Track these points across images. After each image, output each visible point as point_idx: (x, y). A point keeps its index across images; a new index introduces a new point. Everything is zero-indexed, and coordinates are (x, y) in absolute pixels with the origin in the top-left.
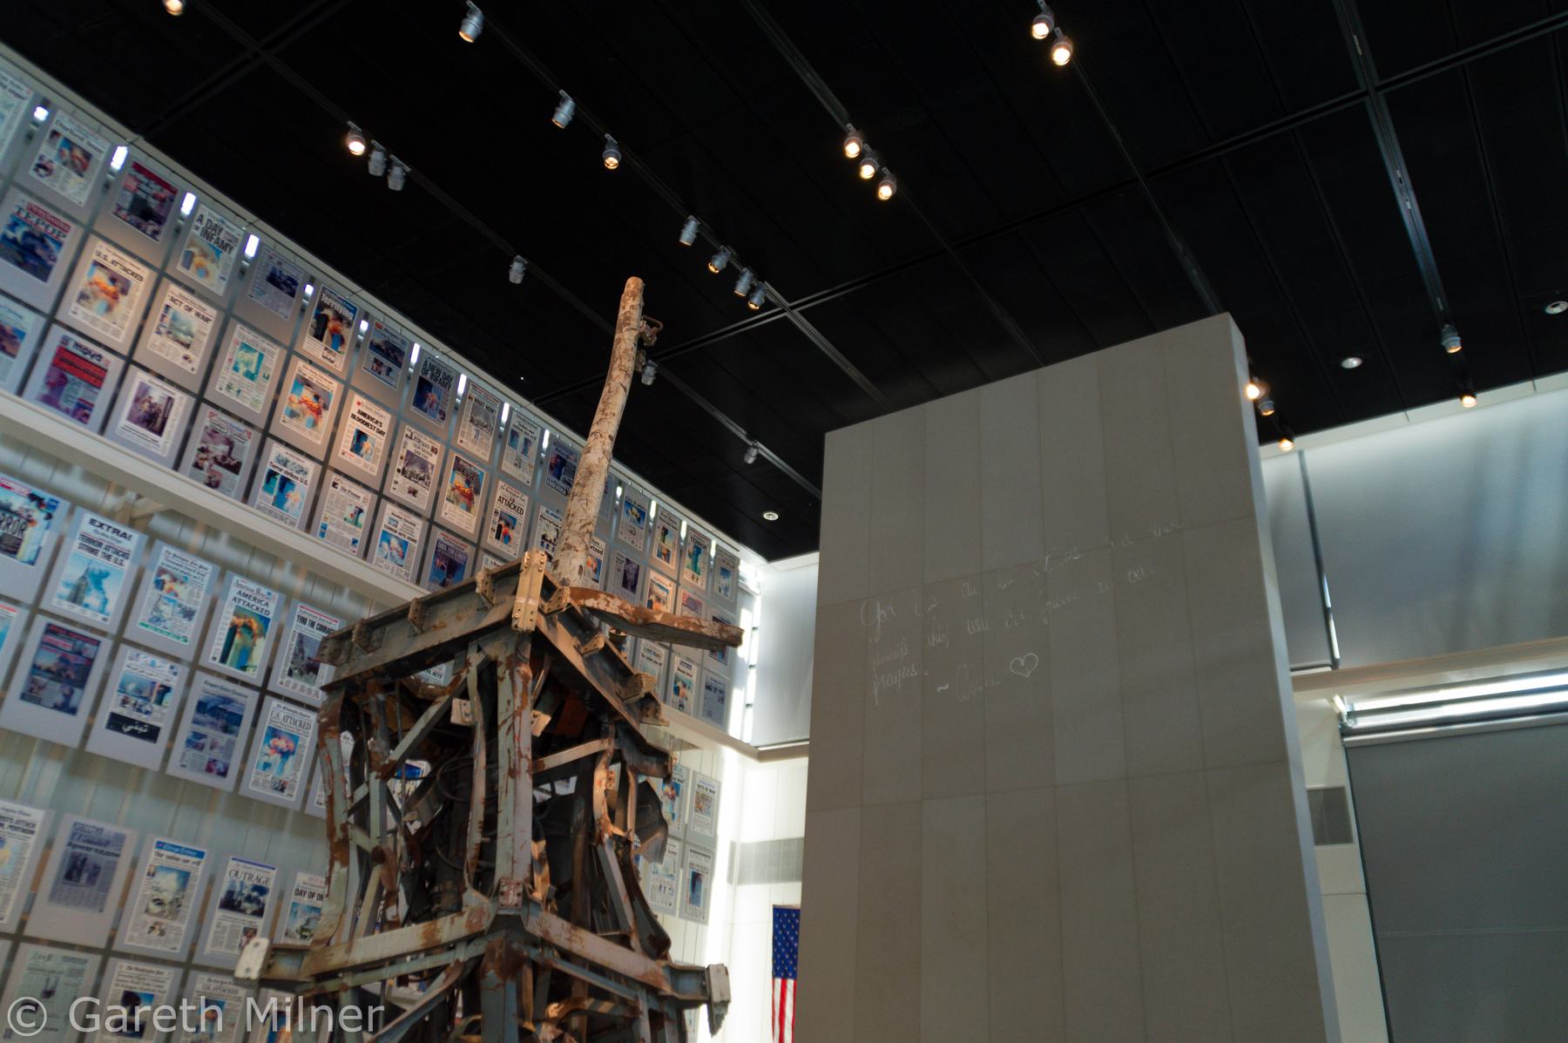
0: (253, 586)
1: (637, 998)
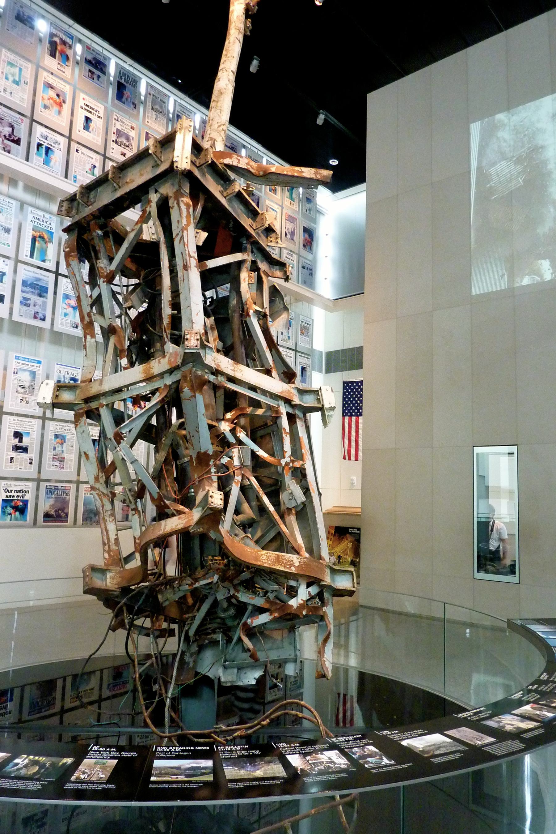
1: (278, 405)
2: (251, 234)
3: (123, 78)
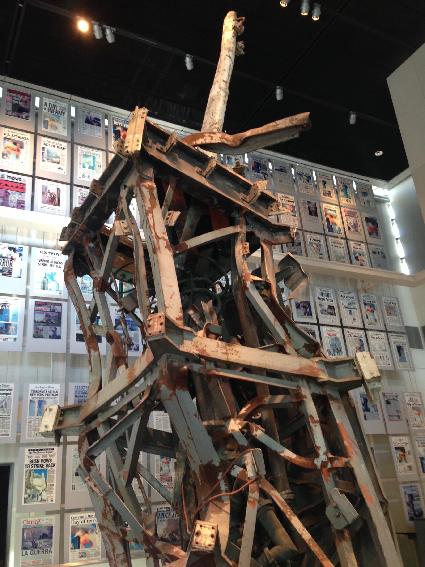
1: (298, 387)
2: (241, 206)
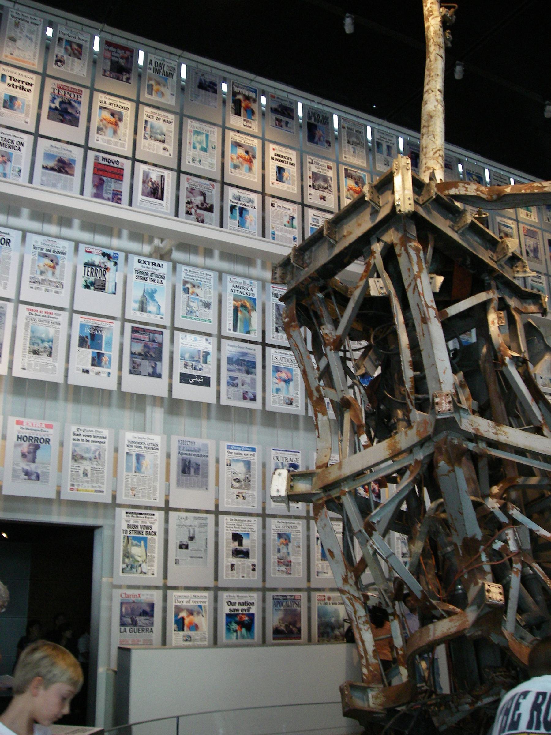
0: (240, 280)
3: (313, 118)
